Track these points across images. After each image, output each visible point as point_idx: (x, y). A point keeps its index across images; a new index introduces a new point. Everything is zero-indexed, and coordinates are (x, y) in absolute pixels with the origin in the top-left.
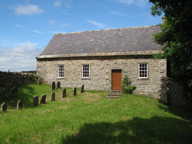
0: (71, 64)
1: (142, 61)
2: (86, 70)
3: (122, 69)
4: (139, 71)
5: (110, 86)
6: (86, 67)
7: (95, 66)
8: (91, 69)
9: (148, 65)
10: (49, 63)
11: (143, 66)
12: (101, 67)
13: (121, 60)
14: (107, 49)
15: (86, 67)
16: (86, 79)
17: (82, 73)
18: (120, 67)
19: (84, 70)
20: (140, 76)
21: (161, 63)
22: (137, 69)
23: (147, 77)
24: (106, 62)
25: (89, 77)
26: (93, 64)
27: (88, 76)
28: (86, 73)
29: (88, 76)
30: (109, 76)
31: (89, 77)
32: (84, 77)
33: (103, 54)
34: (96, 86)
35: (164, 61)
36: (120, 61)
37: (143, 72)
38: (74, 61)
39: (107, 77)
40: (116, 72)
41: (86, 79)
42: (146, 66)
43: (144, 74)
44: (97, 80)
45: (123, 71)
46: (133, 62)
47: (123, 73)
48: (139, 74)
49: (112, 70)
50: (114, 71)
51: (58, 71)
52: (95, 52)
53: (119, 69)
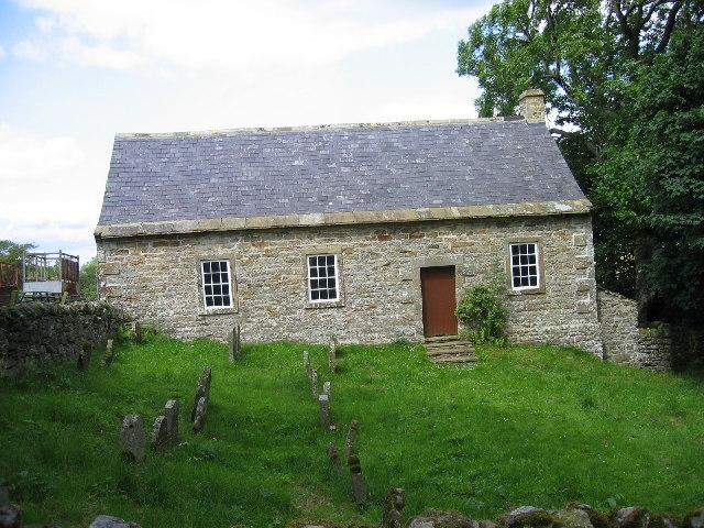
0: (258, 256)
1: (521, 234)
2: (525, 269)
3: (457, 264)
4: (537, 265)
5: (420, 324)
6: (323, 263)
7: (356, 263)
8: (341, 269)
9: (540, 249)
10: (157, 256)
11: (524, 251)
12: (381, 261)
13: (451, 236)
14: (521, 191)
15: (524, 251)
16: (327, 307)
17: (307, 284)
18: (451, 259)
19: (207, 280)
20: (209, 303)
21: (577, 239)
22: (301, 273)
23: (538, 287)
24: (398, 241)
25: (337, 299)
26: (349, 251)
27: (333, 295)
28: (525, 273)
29: (333, 295)
30: (413, 292)
31: (337, 299)
32: (315, 301)
33: (510, 209)
34: (369, 330)
35: (584, 233)
36: (447, 238)
37: (217, 290)
38: (275, 244)
39: (405, 294)
40: (436, 278)
41: (327, 307)
42: (532, 249)
43: (529, 276)
44: (368, 309)
45: (459, 272)
46: (492, 239)
47: (458, 276)
48: (538, 276)
49: (423, 270)
50: (428, 273)
51: (230, 283)
52: (282, 210)
53: (447, 264)
